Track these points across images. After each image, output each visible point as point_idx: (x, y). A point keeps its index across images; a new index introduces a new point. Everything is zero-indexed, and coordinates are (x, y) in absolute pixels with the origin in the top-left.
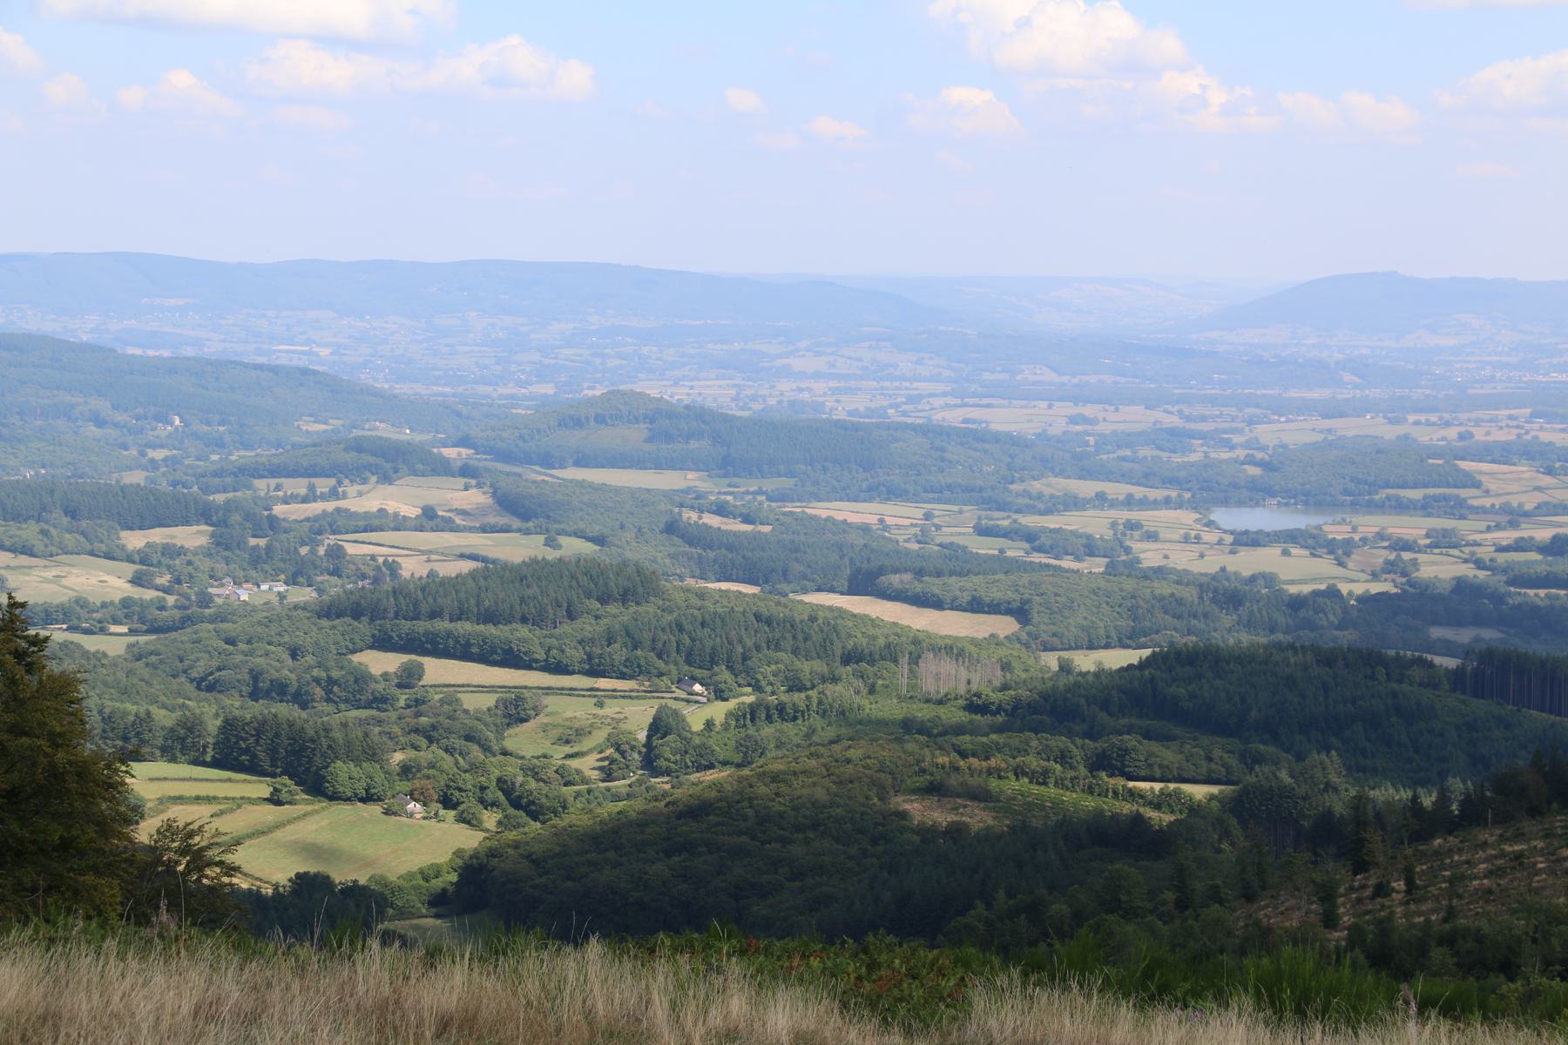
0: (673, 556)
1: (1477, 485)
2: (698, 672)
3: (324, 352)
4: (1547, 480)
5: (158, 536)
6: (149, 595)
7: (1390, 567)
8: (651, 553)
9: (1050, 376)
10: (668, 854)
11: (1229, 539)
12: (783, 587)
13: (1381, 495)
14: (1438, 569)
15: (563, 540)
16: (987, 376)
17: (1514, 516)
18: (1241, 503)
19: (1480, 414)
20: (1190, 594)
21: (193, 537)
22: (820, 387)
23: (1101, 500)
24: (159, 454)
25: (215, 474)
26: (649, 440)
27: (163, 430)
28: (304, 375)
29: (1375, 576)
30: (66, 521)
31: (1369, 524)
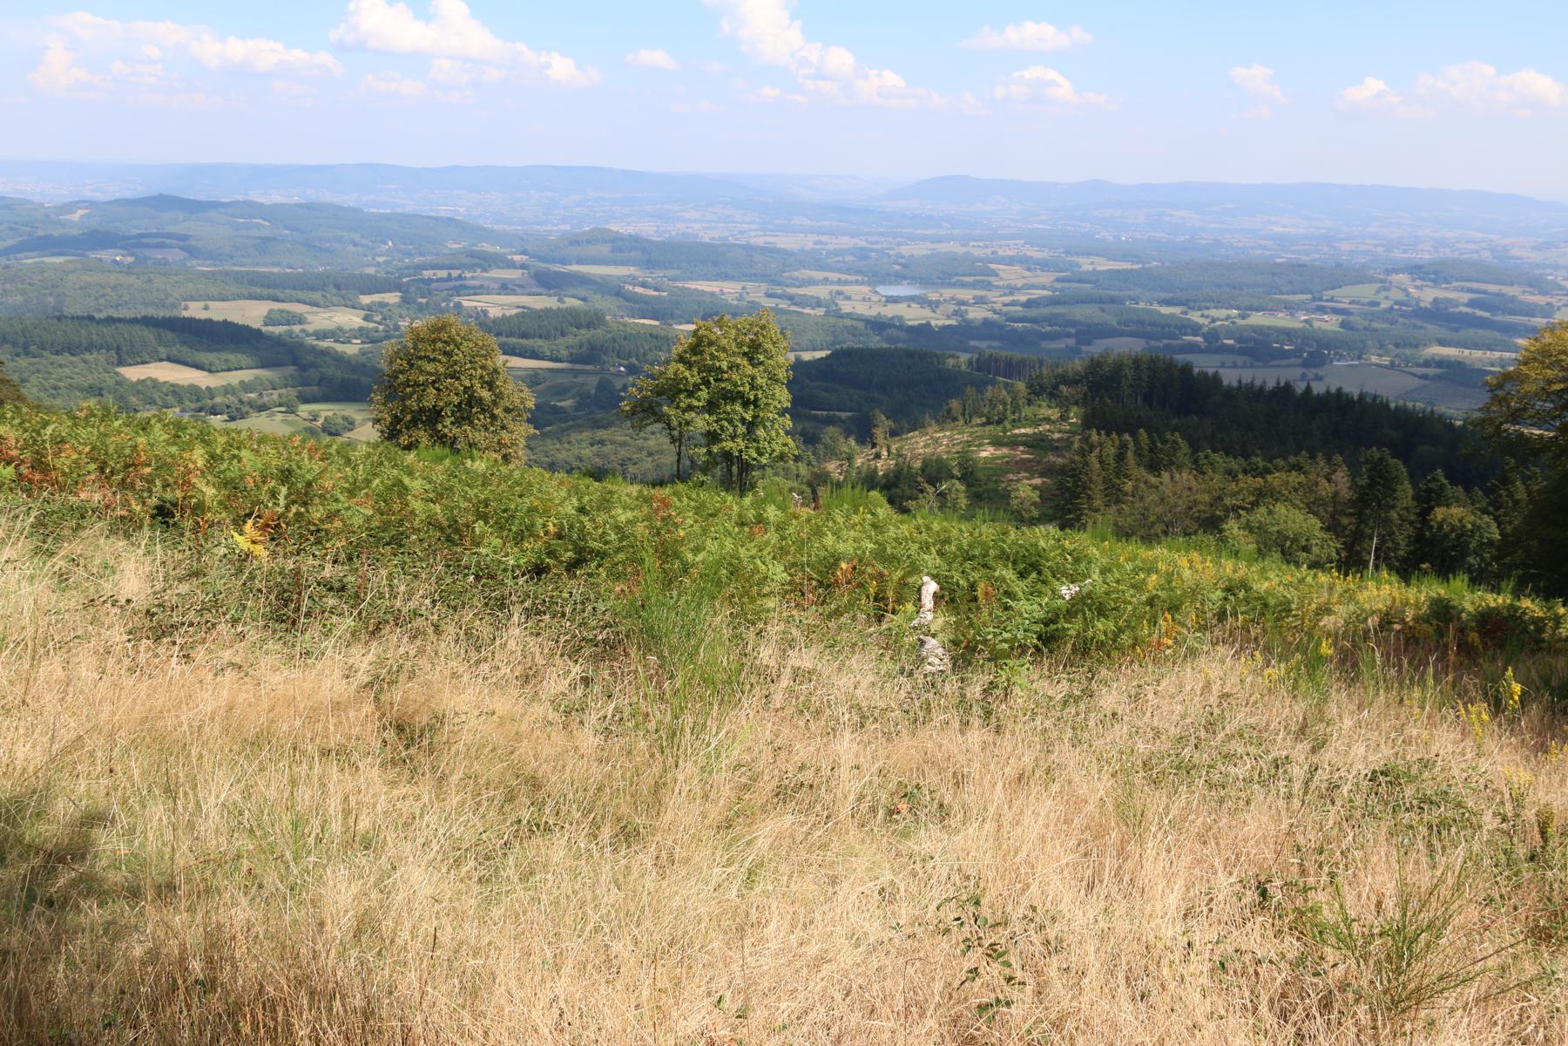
0: (619, 307)
1: (997, 275)
2: (622, 362)
3: (462, 210)
4: (1027, 273)
5: (377, 298)
6: (371, 325)
7: (955, 313)
8: (601, 303)
9: (807, 222)
10: (592, 445)
11: (884, 299)
12: (670, 321)
13: (954, 279)
14: (977, 314)
15: (566, 299)
16: (777, 222)
17: (1012, 290)
18: (890, 283)
19: (1003, 242)
20: (861, 325)
21: (392, 298)
22: (697, 226)
23: (826, 281)
24: (381, 259)
25: (407, 268)
26: (612, 251)
27: (384, 248)
28: (450, 221)
29: (948, 317)
30: (334, 291)
31: (948, 293)
